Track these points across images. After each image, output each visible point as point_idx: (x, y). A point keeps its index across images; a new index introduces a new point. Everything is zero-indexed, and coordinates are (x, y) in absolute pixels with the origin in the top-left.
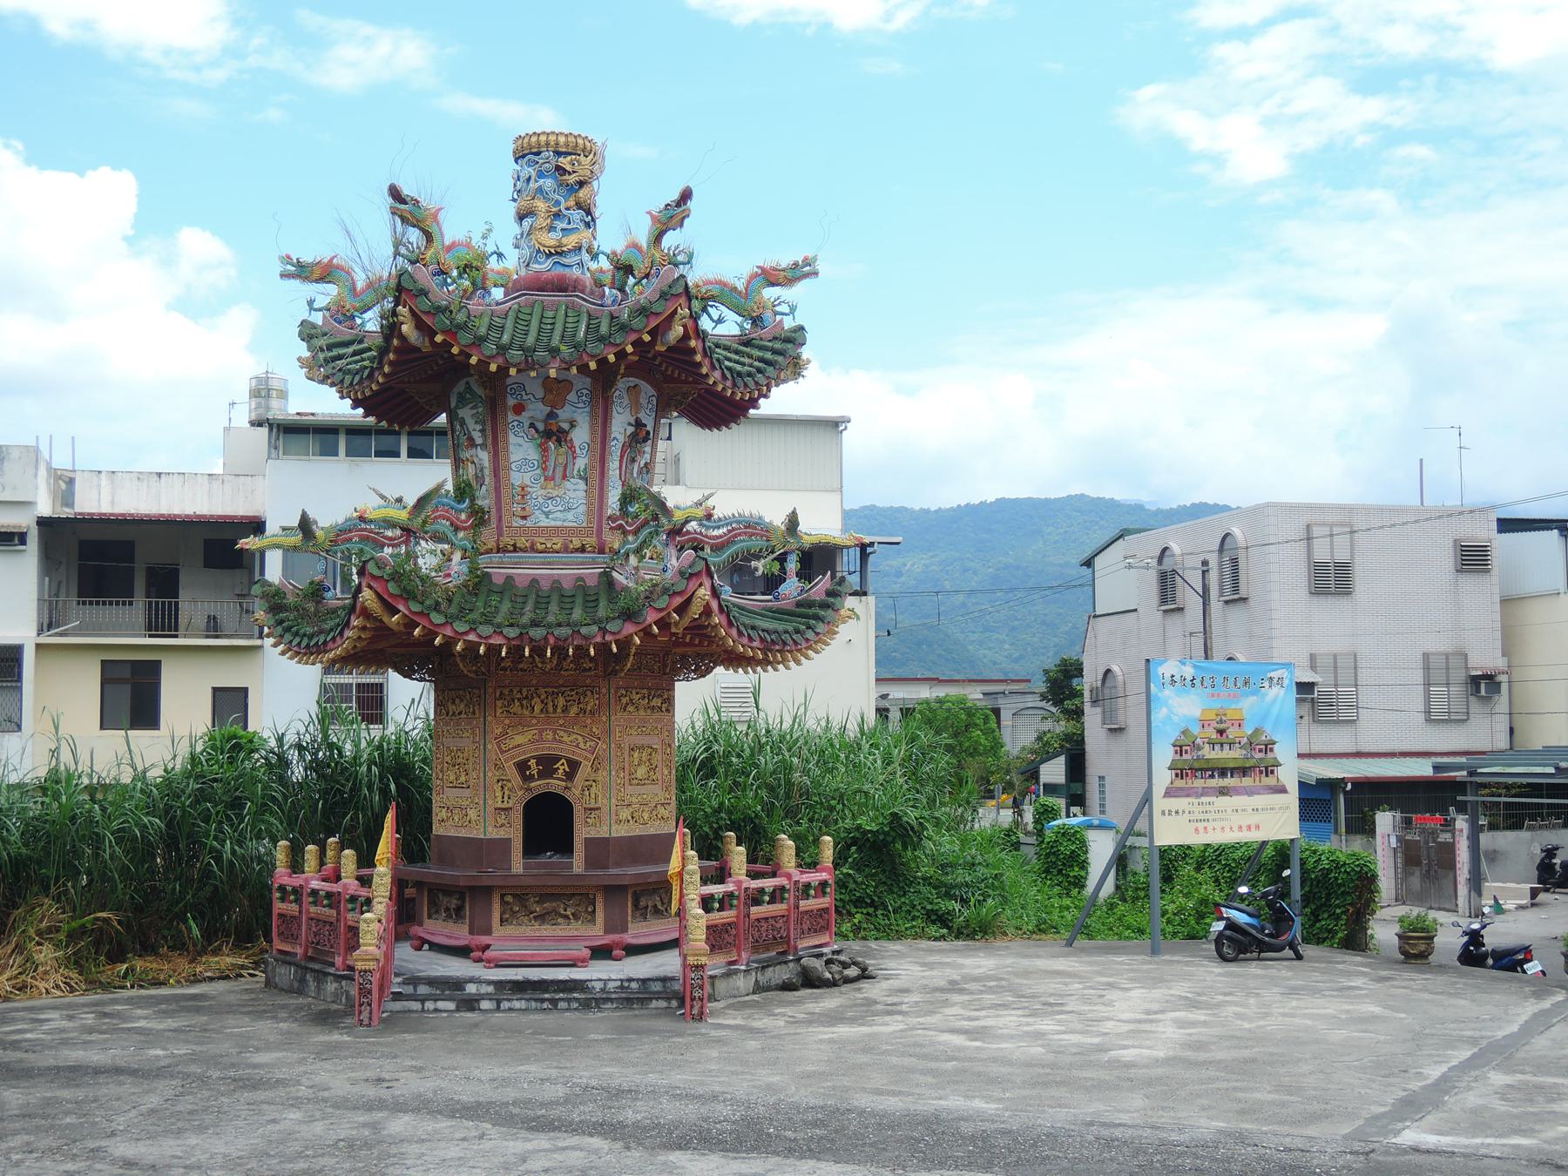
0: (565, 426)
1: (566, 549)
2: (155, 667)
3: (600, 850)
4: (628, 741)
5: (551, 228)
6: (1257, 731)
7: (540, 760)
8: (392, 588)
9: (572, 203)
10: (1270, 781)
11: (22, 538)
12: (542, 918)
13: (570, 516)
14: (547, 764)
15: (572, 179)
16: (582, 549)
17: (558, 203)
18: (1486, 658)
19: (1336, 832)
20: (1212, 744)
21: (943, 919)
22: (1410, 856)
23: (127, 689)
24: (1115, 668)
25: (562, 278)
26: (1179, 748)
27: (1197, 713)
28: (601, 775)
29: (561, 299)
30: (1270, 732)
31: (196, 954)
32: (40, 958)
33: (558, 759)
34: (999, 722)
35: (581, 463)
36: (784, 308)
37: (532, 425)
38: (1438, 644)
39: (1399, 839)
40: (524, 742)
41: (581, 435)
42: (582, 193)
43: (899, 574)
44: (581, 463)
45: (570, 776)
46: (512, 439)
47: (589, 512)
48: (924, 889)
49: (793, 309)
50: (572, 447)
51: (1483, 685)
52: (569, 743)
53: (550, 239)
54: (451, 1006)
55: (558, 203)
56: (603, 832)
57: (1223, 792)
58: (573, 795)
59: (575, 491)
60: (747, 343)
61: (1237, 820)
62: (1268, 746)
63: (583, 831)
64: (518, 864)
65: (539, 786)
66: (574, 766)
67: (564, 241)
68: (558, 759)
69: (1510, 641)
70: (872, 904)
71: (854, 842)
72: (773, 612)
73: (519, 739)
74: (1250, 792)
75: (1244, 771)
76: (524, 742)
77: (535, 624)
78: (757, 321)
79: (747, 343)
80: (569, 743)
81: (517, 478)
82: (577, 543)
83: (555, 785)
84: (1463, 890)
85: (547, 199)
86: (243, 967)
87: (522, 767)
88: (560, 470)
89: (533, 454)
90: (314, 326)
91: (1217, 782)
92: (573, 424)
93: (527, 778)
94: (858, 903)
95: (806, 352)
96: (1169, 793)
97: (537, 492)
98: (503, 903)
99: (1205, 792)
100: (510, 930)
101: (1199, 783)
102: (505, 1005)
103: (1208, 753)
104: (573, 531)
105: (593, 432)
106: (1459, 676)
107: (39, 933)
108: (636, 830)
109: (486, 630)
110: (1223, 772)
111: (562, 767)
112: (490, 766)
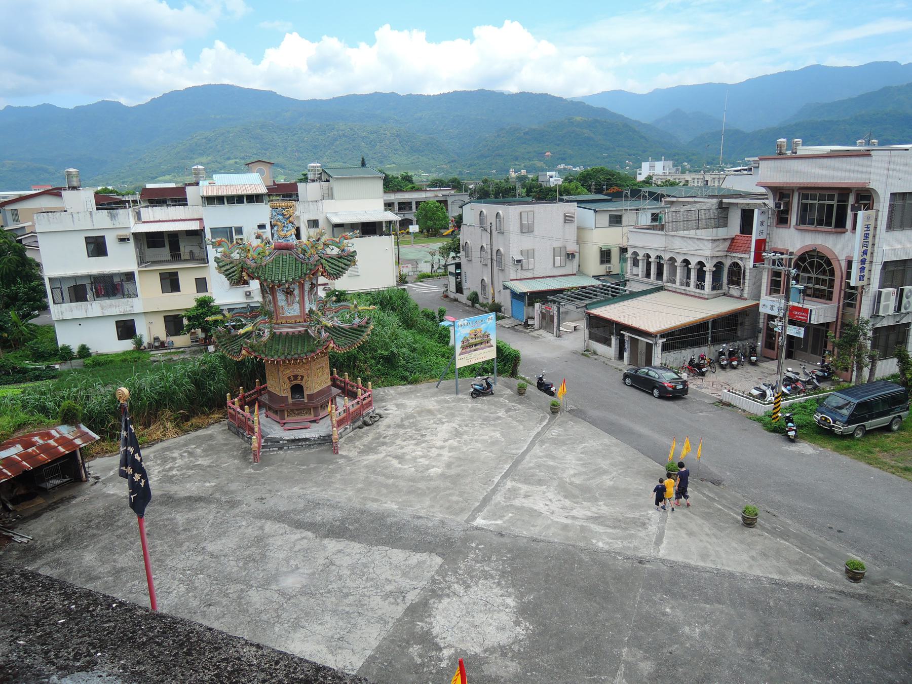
0: (292, 290)
1: (296, 322)
2: (176, 274)
3: (311, 397)
4: (316, 368)
5: (283, 230)
6: (485, 333)
7: (293, 376)
8: (250, 350)
9: (288, 222)
10: (489, 344)
11: (128, 239)
12: (298, 414)
13: (296, 313)
14: (296, 377)
15: (287, 216)
16: (300, 322)
17: (284, 223)
18: (572, 247)
19: (525, 305)
20: (472, 339)
21: (404, 378)
22: (543, 316)
23: (169, 280)
24: (468, 242)
25: (287, 245)
26: (463, 342)
27: (469, 332)
28: (310, 379)
29: (287, 252)
30: (489, 332)
31: (207, 415)
32: (168, 426)
33: (298, 376)
34: (447, 210)
35: (297, 299)
36: (350, 245)
37: (283, 291)
38: (558, 244)
39: (540, 312)
40: (289, 372)
41: (296, 292)
42: (291, 219)
43: (421, 118)
44: (297, 299)
45: (302, 380)
46: (278, 294)
47: (300, 312)
48: (401, 369)
49: (353, 245)
50: (294, 295)
51: (570, 256)
52: (300, 371)
53: (283, 233)
54: (277, 449)
55: (284, 223)
56: (312, 392)
57: (475, 350)
58: (303, 384)
59: (296, 307)
60: (340, 258)
61: (479, 356)
62: (488, 336)
63: (306, 392)
64: (290, 401)
65: (294, 382)
66: (302, 377)
67: (287, 234)
68: (298, 376)
69: (579, 242)
70: (387, 374)
71: (382, 357)
72: (352, 329)
73: (288, 372)
74: (483, 348)
75: (481, 343)
76: (289, 372)
77: (288, 354)
78: (343, 251)
79: (340, 258)
80: (300, 371)
81: (280, 304)
82: (298, 321)
83: (298, 382)
84: (555, 329)
85: (280, 221)
86: (221, 418)
87: (289, 378)
88: (291, 302)
89: (284, 298)
90: (218, 258)
91: (474, 348)
92: (294, 289)
93: (291, 381)
94: (383, 374)
95: (357, 258)
96: (460, 354)
97: (286, 308)
98: (287, 412)
99: (470, 351)
100: (290, 418)
101: (469, 349)
102: (290, 447)
103: (471, 341)
104: (297, 317)
105: (300, 292)
106: (563, 253)
107: (166, 419)
108: (320, 388)
109: (276, 357)
110: (475, 345)
111: (299, 377)
112: (281, 379)
